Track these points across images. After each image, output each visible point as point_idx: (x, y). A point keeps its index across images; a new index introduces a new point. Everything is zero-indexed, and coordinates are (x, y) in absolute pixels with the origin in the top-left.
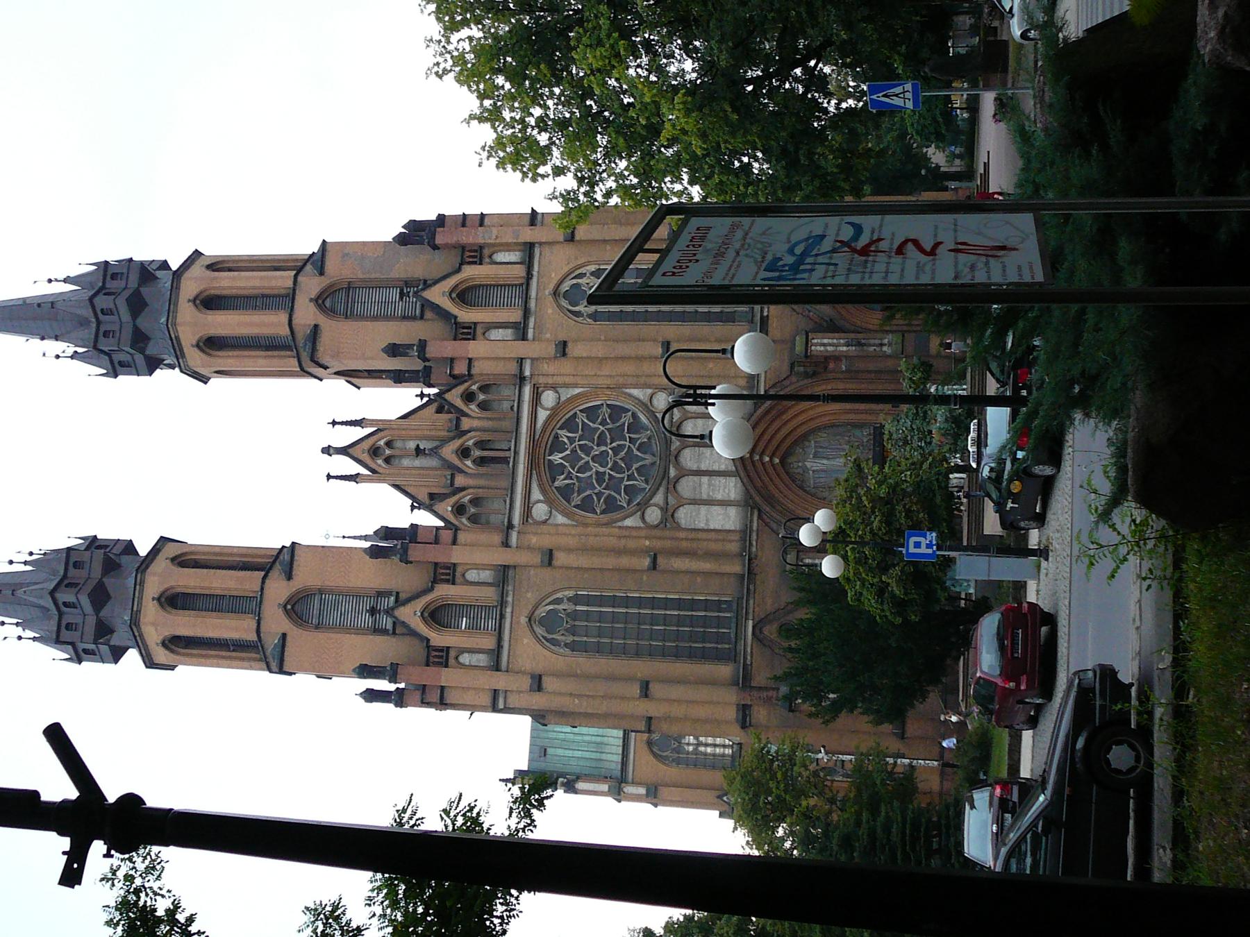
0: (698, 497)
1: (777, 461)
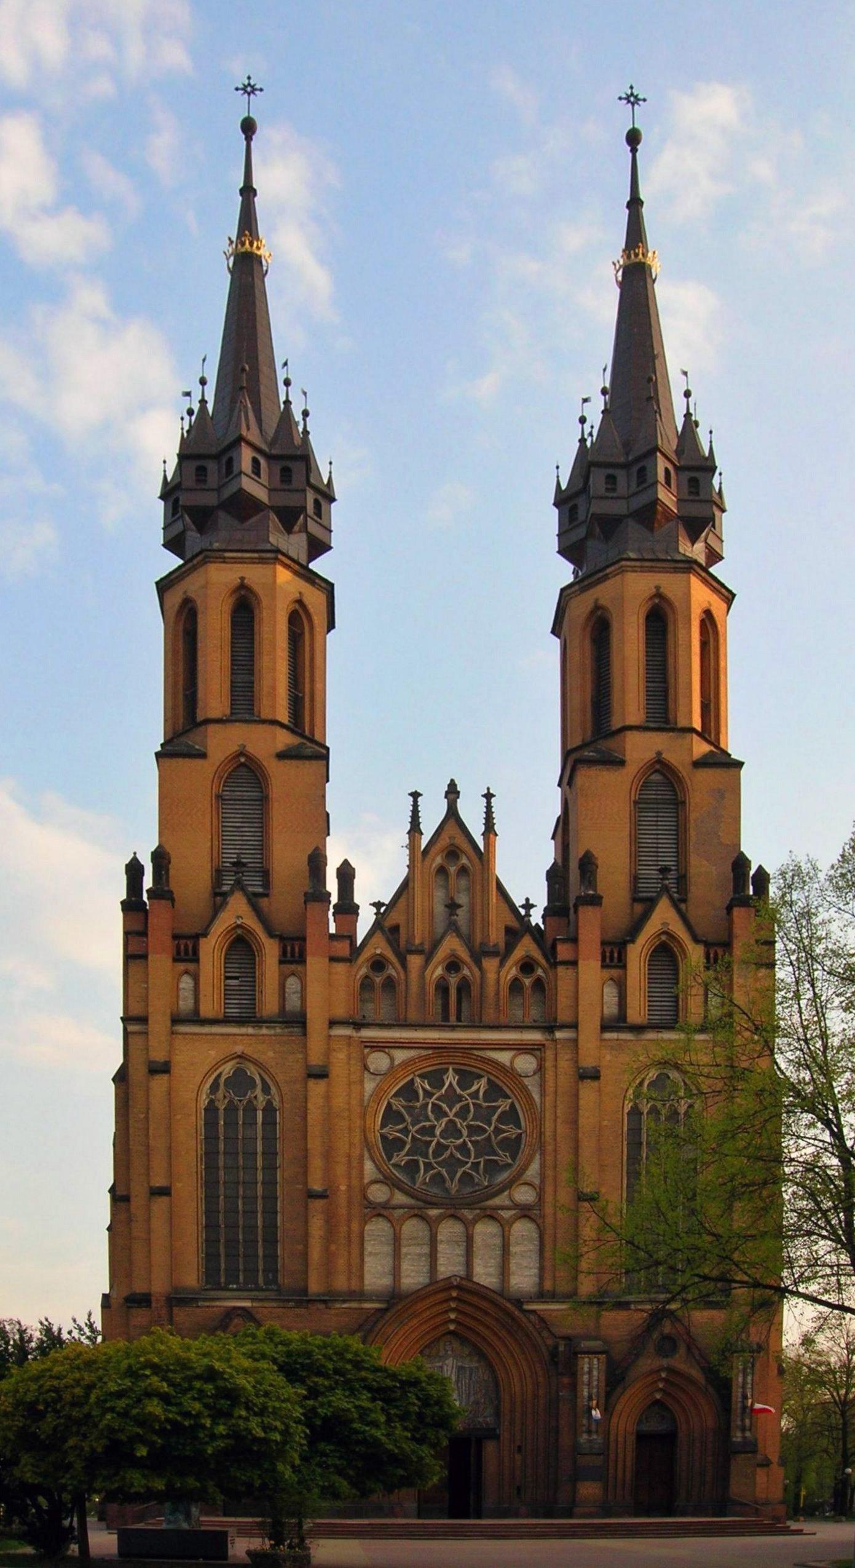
0: (404, 1242)
1: (452, 1327)
